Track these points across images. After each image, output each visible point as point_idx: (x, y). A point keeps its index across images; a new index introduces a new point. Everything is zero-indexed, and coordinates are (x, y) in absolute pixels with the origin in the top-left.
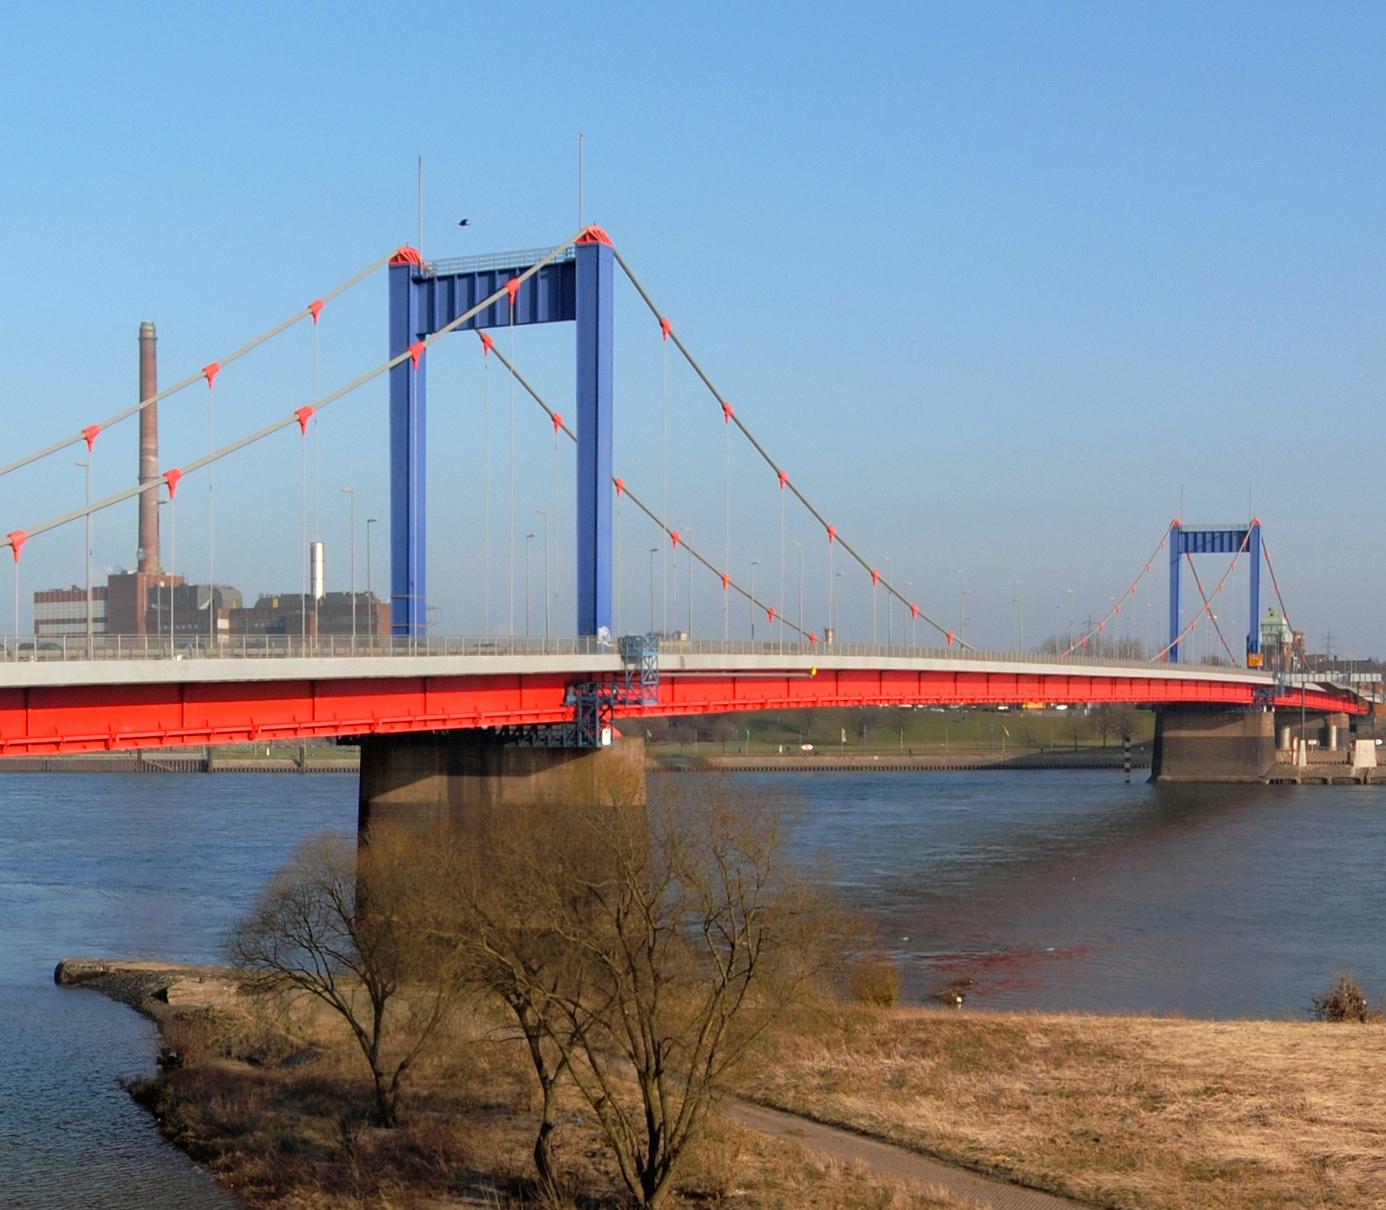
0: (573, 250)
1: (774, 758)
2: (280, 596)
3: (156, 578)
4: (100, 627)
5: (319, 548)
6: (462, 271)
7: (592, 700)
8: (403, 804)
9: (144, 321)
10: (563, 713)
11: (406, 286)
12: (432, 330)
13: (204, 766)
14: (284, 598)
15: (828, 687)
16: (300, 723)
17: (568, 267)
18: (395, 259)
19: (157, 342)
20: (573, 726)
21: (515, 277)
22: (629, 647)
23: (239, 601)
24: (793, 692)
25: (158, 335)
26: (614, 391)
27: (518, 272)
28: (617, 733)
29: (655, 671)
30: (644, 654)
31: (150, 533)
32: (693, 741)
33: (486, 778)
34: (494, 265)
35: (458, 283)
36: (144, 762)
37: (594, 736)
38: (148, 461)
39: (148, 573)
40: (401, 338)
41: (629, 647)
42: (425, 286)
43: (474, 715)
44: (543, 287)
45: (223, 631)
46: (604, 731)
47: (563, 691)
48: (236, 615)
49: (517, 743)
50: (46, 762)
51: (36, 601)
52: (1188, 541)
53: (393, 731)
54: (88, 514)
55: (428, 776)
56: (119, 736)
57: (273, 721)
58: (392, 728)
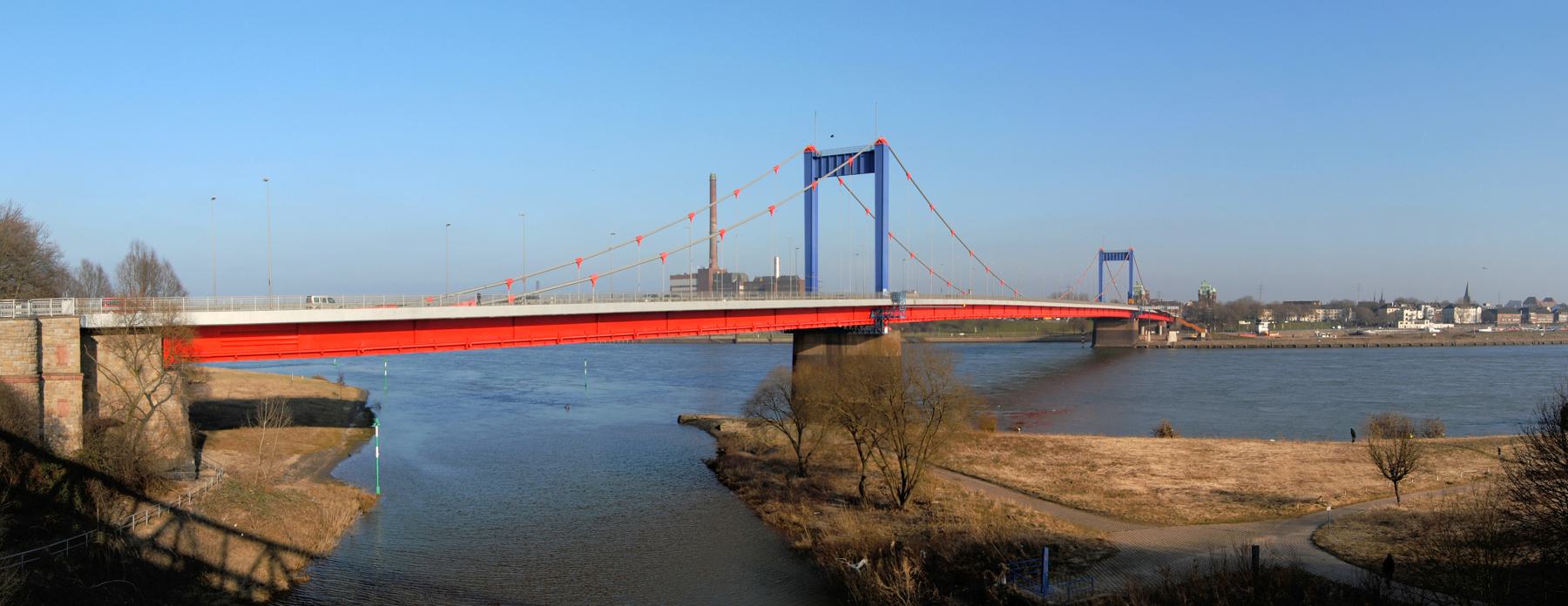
5: (778, 259)
12: (820, 177)
13: (734, 341)
14: (764, 278)
22: (894, 296)
23: (747, 279)
31: (714, 253)
35: (822, 160)
40: (809, 179)
41: (894, 296)
44: (862, 160)
48: (746, 284)
52: (1106, 256)
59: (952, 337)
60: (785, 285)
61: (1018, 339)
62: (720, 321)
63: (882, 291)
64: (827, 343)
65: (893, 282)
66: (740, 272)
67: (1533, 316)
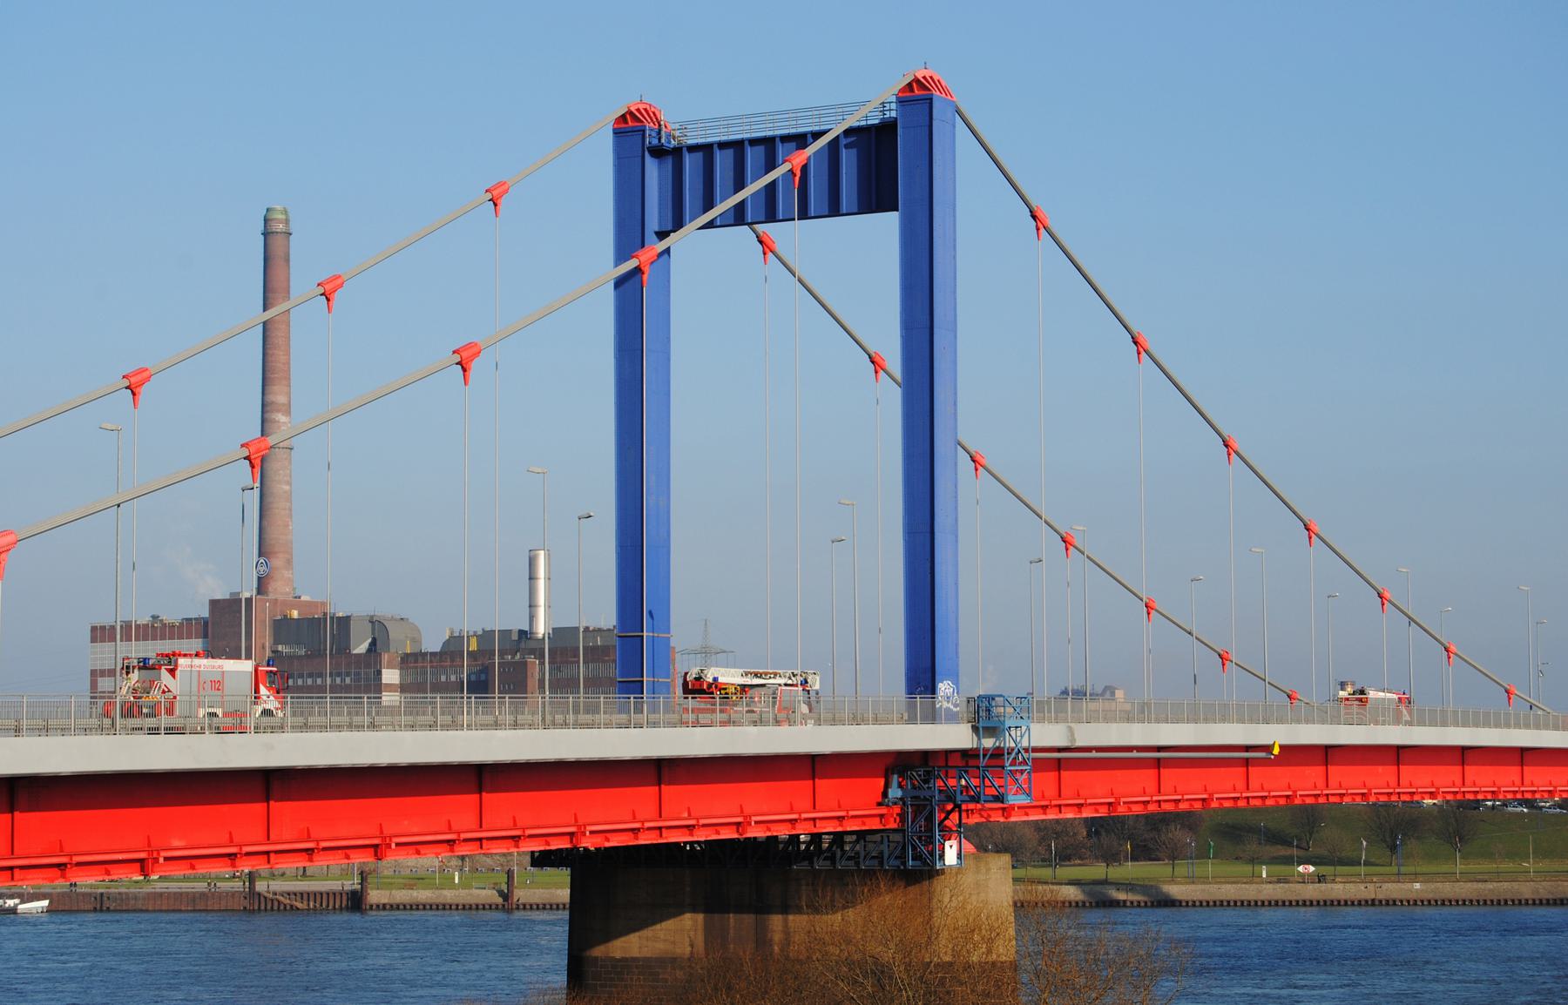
0: (894, 106)
1: (1254, 886)
2: (480, 633)
3: (284, 603)
5: (542, 555)
6: (724, 138)
7: (927, 794)
8: (634, 959)
9: (268, 206)
10: (882, 816)
11: (640, 159)
12: (678, 224)
13: (355, 901)
15: (1146, 777)
16: (459, 833)
17: (886, 130)
19: (291, 237)
20: (897, 837)
21: (805, 146)
22: (983, 714)
23: (416, 641)
24: (1166, 785)
25: (293, 228)
26: (958, 318)
27: (810, 139)
28: (968, 847)
29: (1026, 750)
30: (1007, 724)
31: (274, 533)
32: (1126, 860)
33: (766, 916)
34: (774, 129)
35: (718, 156)
36: (259, 894)
37: (932, 853)
38: (275, 421)
39: (271, 596)
40: (630, 235)
41: (983, 714)
42: (669, 162)
43: (740, 819)
44: (848, 159)
45: (390, 687)
46: (947, 844)
47: (882, 782)
48: (409, 661)
49: (811, 863)
50: (102, 894)
51: (94, 640)
53: (607, 844)
54: (119, 506)
55: (674, 915)
56: (164, 854)
57: (415, 830)
58: (608, 840)
59: (1262, 883)
61: (1544, 889)
62: (243, 820)
63: (933, 690)
64: (708, 909)
66: (383, 610)
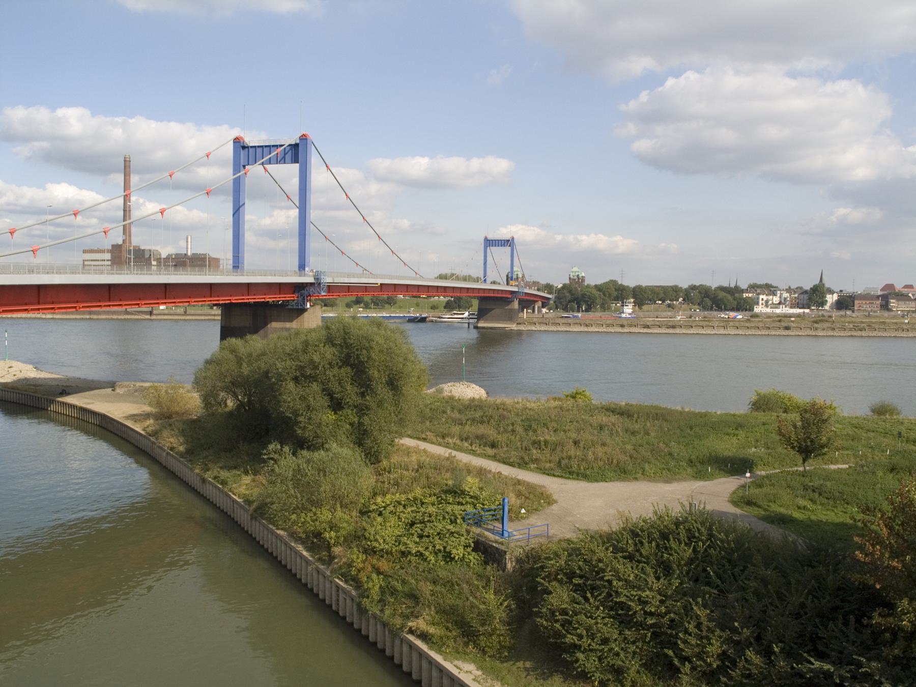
4: (109, 263)
17: (296, 146)
18: (235, 139)
45: (154, 265)
52: (489, 243)
60: (477, 280)
65: (314, 263)
67: (893, 303)
